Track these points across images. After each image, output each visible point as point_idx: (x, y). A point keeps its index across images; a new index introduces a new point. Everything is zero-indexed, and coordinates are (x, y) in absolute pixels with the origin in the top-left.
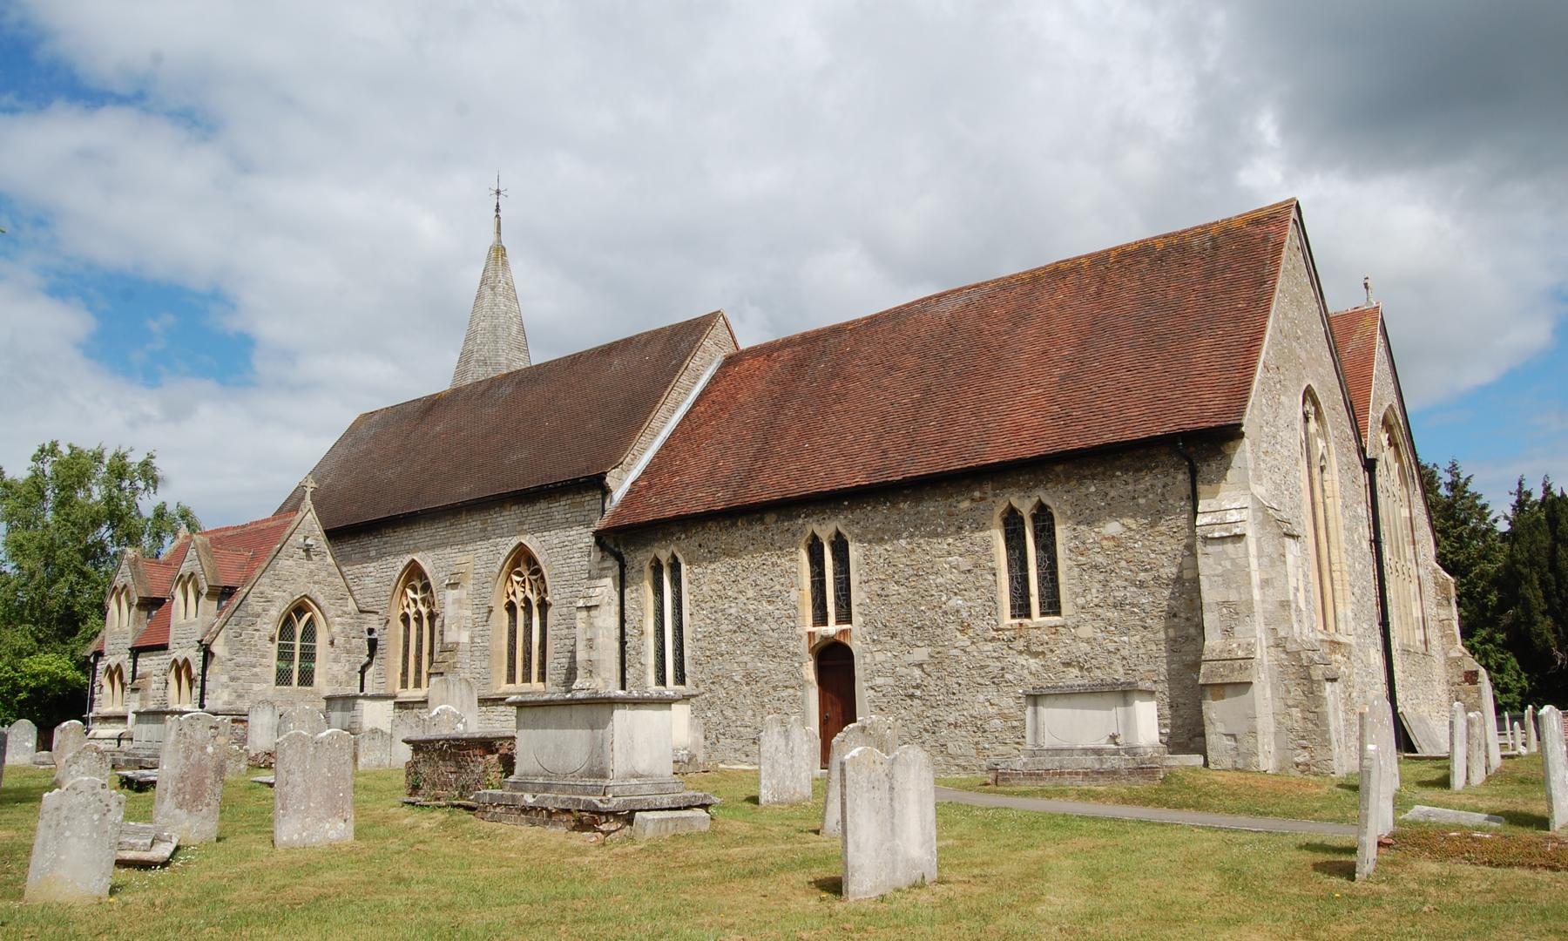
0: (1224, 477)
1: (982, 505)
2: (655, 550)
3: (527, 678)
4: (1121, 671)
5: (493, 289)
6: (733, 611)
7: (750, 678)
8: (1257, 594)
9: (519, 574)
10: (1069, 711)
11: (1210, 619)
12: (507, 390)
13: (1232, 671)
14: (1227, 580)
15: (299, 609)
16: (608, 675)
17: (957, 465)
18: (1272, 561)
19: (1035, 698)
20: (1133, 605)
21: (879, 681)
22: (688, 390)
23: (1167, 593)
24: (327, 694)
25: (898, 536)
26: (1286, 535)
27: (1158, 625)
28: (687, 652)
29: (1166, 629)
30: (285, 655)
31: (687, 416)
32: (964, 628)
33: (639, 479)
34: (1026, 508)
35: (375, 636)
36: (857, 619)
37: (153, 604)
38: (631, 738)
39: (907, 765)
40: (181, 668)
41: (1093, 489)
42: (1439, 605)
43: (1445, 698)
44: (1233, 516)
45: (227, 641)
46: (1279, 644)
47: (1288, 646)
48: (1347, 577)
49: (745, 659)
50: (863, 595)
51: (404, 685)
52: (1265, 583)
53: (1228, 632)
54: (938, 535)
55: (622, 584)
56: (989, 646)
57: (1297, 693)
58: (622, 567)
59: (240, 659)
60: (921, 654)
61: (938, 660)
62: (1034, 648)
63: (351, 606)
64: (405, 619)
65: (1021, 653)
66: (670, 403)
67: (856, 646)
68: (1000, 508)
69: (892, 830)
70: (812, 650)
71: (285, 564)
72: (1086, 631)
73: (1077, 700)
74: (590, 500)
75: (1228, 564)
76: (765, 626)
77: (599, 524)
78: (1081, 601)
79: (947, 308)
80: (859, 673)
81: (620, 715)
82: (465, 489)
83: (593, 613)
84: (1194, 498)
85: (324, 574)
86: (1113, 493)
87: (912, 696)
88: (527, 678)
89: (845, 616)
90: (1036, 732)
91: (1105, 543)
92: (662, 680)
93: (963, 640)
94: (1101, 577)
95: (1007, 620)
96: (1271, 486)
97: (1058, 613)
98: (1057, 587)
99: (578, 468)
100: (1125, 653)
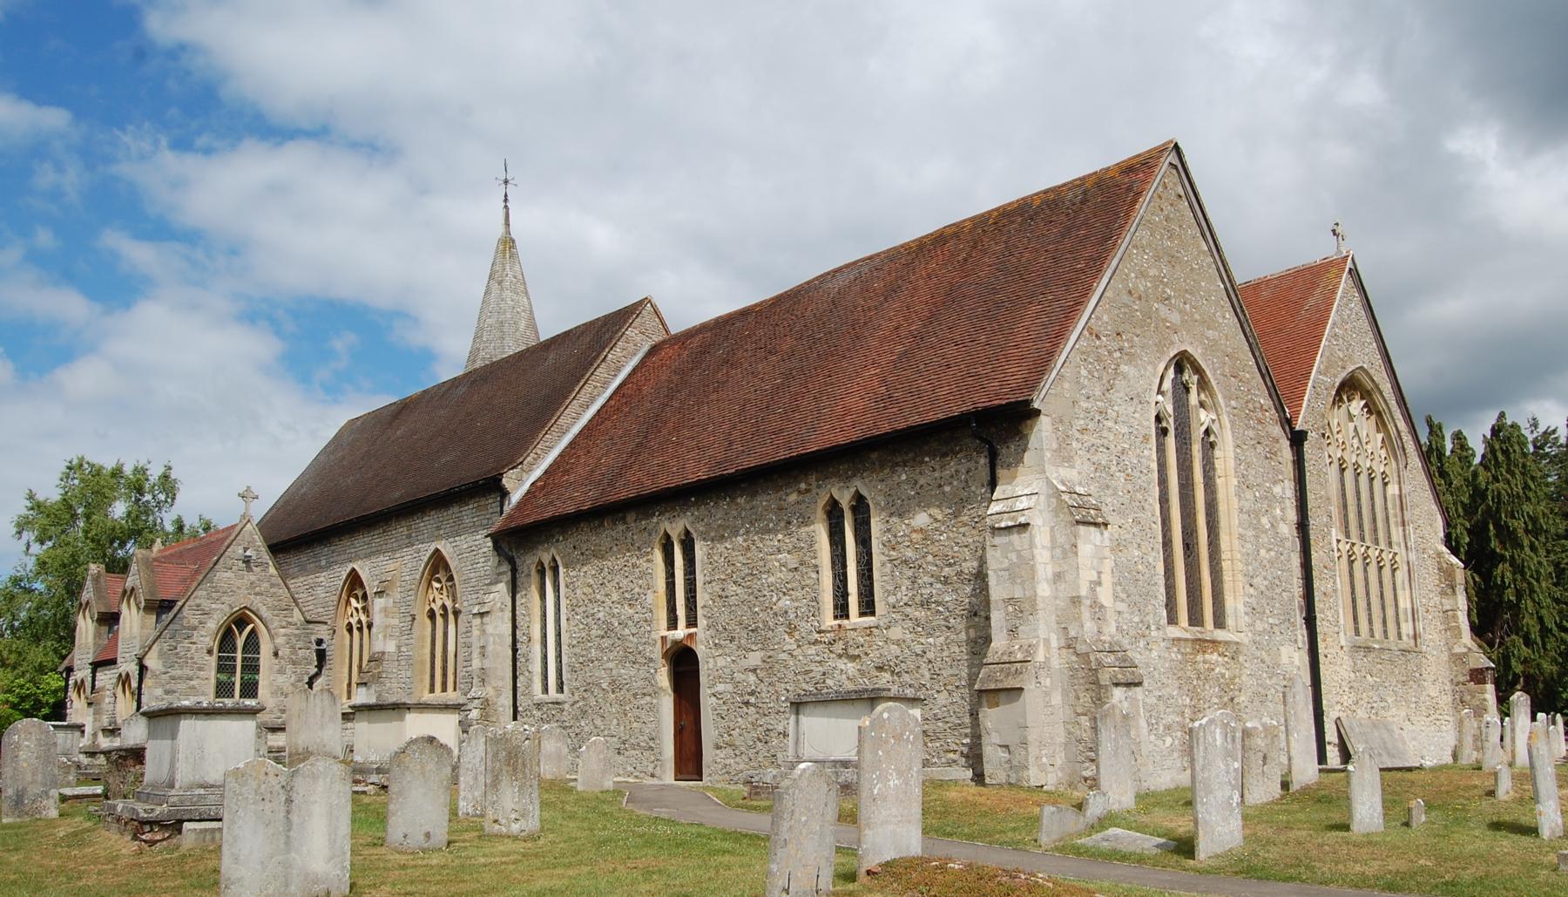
0: (1021, 460)
1: (807, 498)
2: (540, 553)
3: (444, 689)
4: (928, 676)
5: (500, 283)
6: (601, 615)
7: (615, 685)
8: (1044, 590)
9: (439, 581)
10: (825, 720)
11: (997, 617)
12: (462, 390)
13: (1007, 675)
14: (1012, 573)
15: (241, 621)
16: (500, 683)
17: (783, 454)
18: (1064, 552)
19: (797, 706)
20: (938, 603)
21: (720, 687)
22: (606, 384)
23: (968, 589)
24: (1138, 689)
25: (736, 534)
26: (1078, 522)
27: (959, 624)
28: (565, 659)
29: (968, 628)
30: (225, 667)
31: (603, 406)
32: (791, 629)
33: (539, 479)
34: (845, 500)
35: (324, 646)
36: (702, 622)
37: (109, 620)
38: (201, 749)
39: (315, 777)
40: (124, 680)
41: (904, 477)
42: (1443, 593)
43: (1446, 700)
44: (1021, 504)
45: (161, 654)
46: (1069, 645)
47: (1078, 647)
48: (1240, 566)
49: (611, 665)
50: (707, 597)
51: (432, 690)
52: (1058, 577)
53: (1013, 631)
54: (769, 531)
55: (514, 590)
56: (812, 650)
57: (1085, 698)
58: (514, 571)
59: (177, 672)
60: (755, 659)
61: (769, 664)
62: (851, 651)
63: (297, 616)
64: (350, 628)
65: (840, 656)
66: (583, 397)
67: (700, 650)
68: (822, 501)
69: (287, 843)
70: (665, 656)
71: (223, 576)
72: (896, 633)
73: (832, 708)
74: (492, 502)
75: (1013, 556)
76: (627, 631)
77: (498, 523)
78: (892, 599)
79: (841, 281)
80: (703, 679)
81: (186, 725)
82: (397, 494)
83: (486, 619)
84: (993, 484)
85: (266, 585)
86: (922, 481)
87: (747, 703)
88: (444, 689)
89: (692, 622)
90: (797, 742)
91: (914, 535)
92: (546, 690)
93: (790, 643)
94: (910, 573)
95: (829, 621)
96: (1088, 468)
97: (873, 613)
98: (872, 584)
99: (471, 472)
100: (930, 655)
